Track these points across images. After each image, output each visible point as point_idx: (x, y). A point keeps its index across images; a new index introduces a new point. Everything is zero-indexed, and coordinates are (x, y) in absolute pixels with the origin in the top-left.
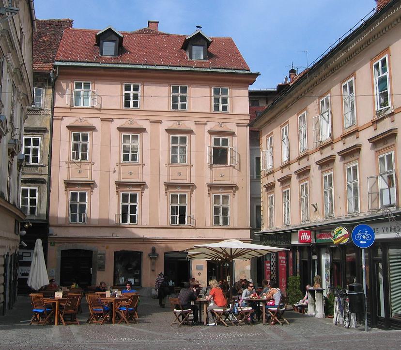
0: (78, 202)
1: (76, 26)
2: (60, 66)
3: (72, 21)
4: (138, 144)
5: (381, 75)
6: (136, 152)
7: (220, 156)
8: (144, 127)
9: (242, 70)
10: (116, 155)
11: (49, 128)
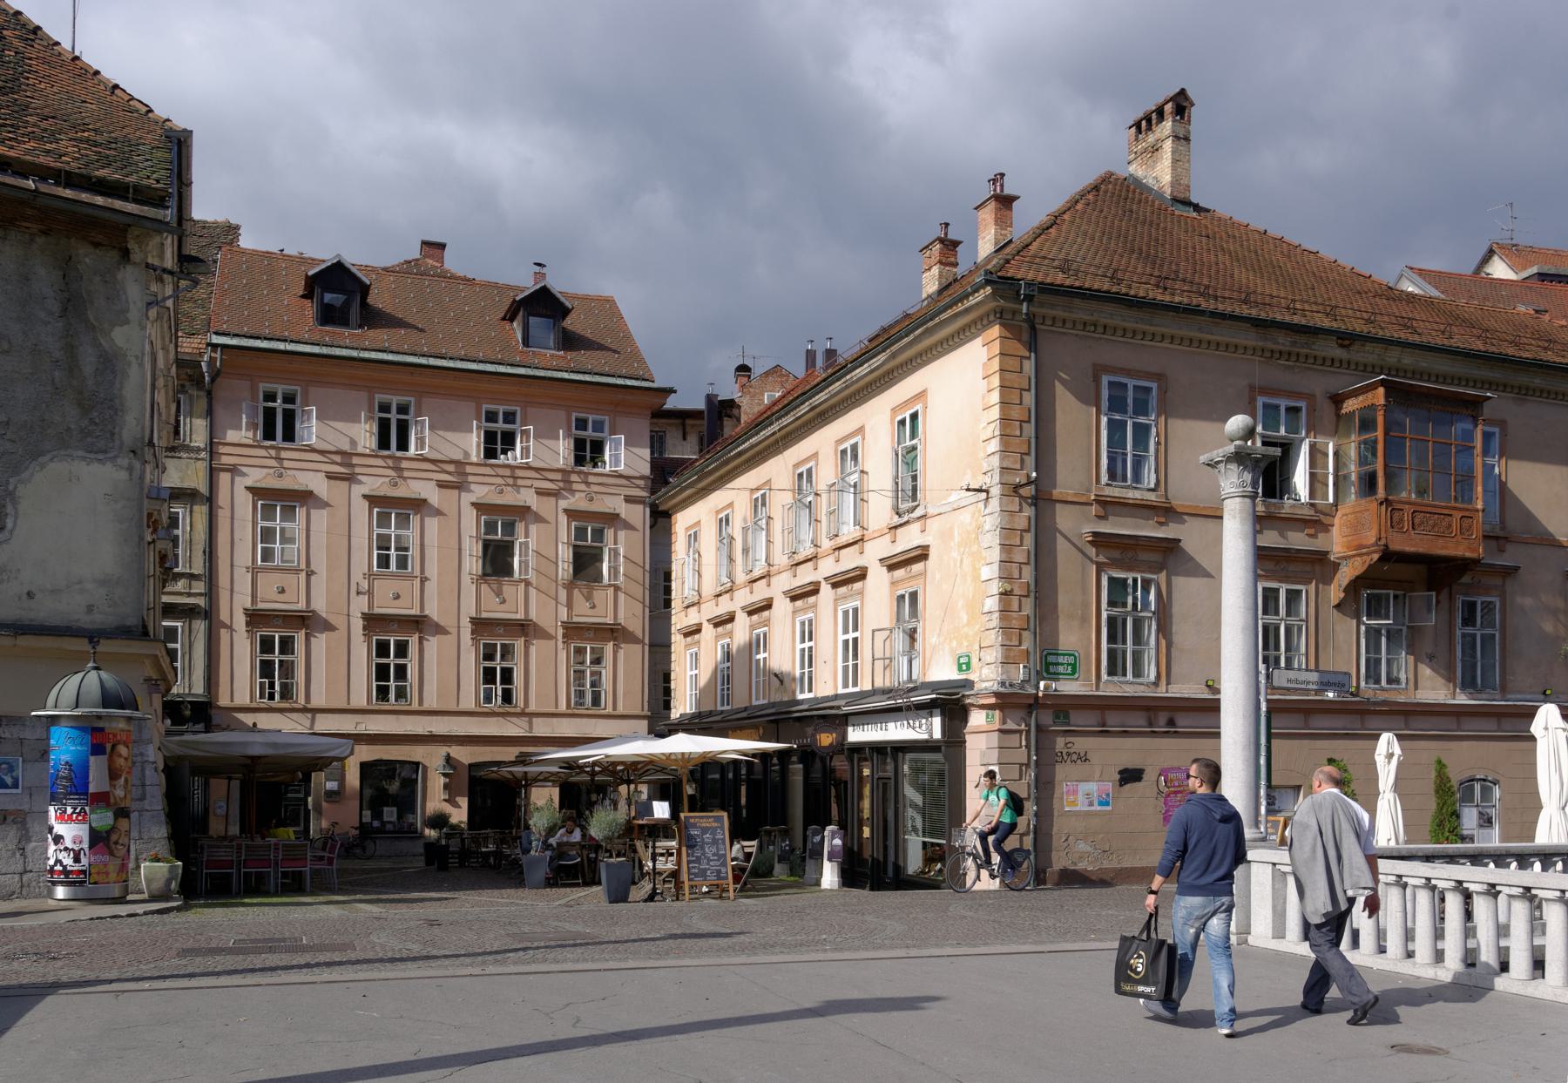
1: (246, 242)
2: (224, 346)
3: (237, 228)
4: (412, 535)
5: (908, 443)
6: (406, 549)
7: (585, 563)
8: (423, 496)
9: (637, 379)
10: (363, 557)
11: (203, 488)
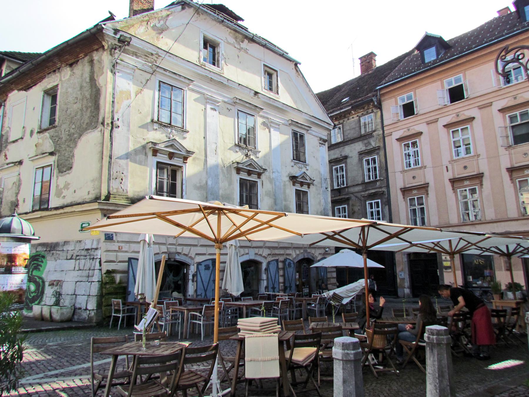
0: (417, 207)
6: (469, 144)
